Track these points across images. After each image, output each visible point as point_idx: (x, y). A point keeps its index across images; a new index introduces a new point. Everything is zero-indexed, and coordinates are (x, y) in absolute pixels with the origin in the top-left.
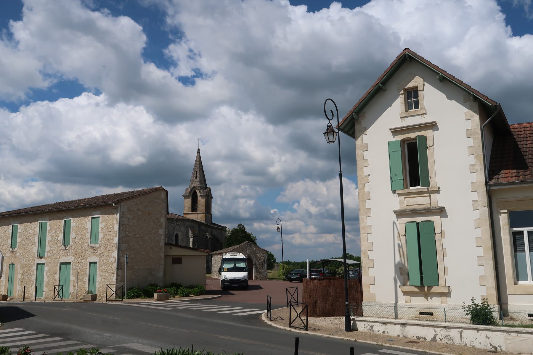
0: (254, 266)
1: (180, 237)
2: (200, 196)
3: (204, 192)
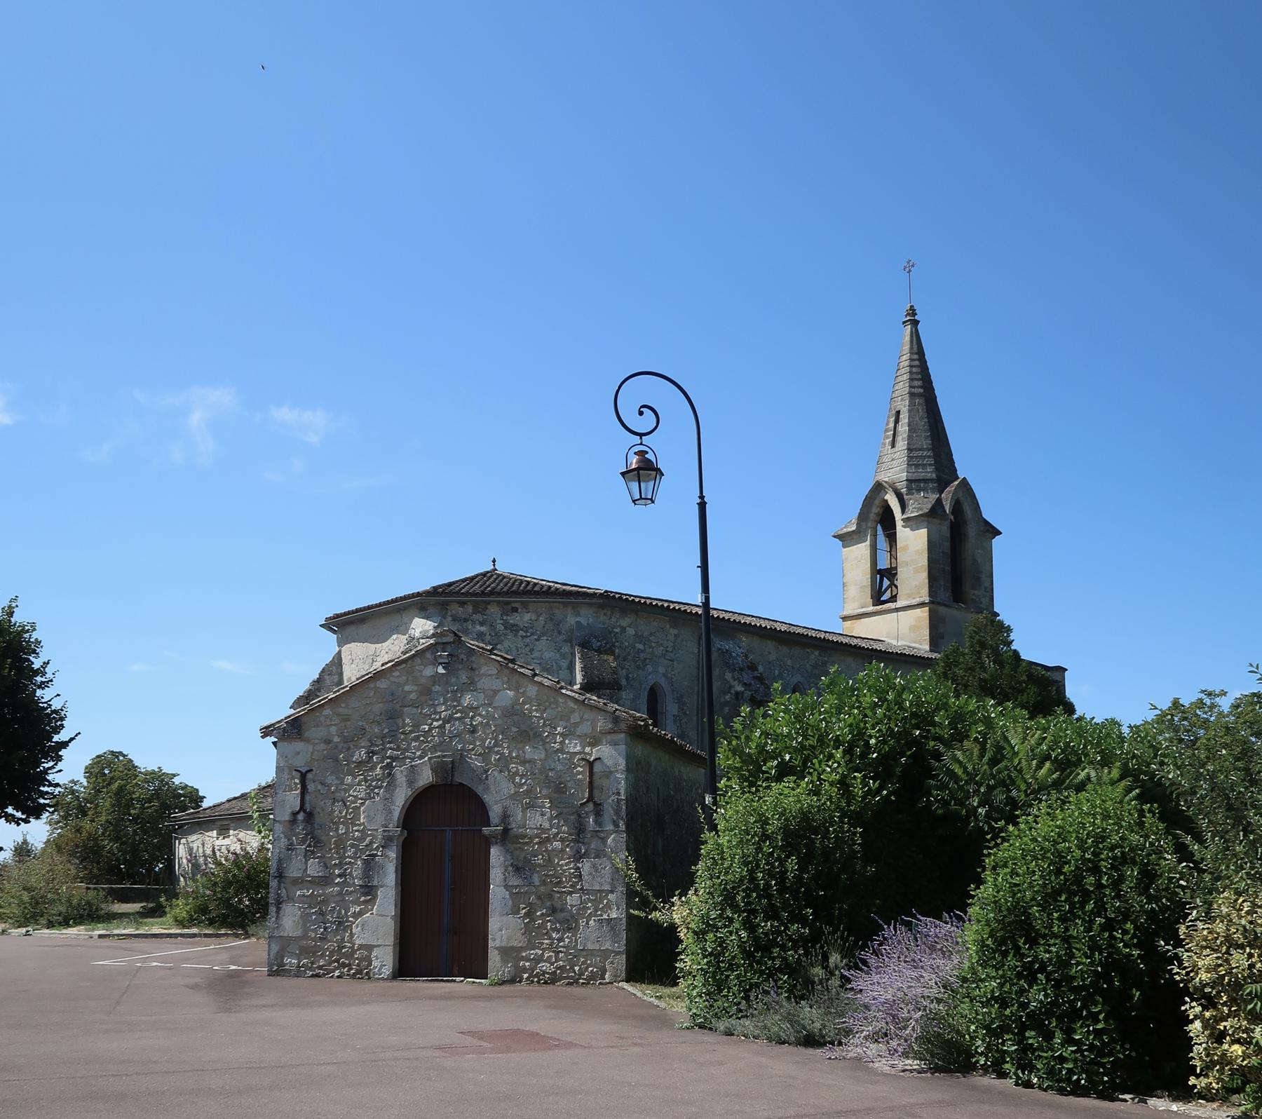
0: (496, 854)
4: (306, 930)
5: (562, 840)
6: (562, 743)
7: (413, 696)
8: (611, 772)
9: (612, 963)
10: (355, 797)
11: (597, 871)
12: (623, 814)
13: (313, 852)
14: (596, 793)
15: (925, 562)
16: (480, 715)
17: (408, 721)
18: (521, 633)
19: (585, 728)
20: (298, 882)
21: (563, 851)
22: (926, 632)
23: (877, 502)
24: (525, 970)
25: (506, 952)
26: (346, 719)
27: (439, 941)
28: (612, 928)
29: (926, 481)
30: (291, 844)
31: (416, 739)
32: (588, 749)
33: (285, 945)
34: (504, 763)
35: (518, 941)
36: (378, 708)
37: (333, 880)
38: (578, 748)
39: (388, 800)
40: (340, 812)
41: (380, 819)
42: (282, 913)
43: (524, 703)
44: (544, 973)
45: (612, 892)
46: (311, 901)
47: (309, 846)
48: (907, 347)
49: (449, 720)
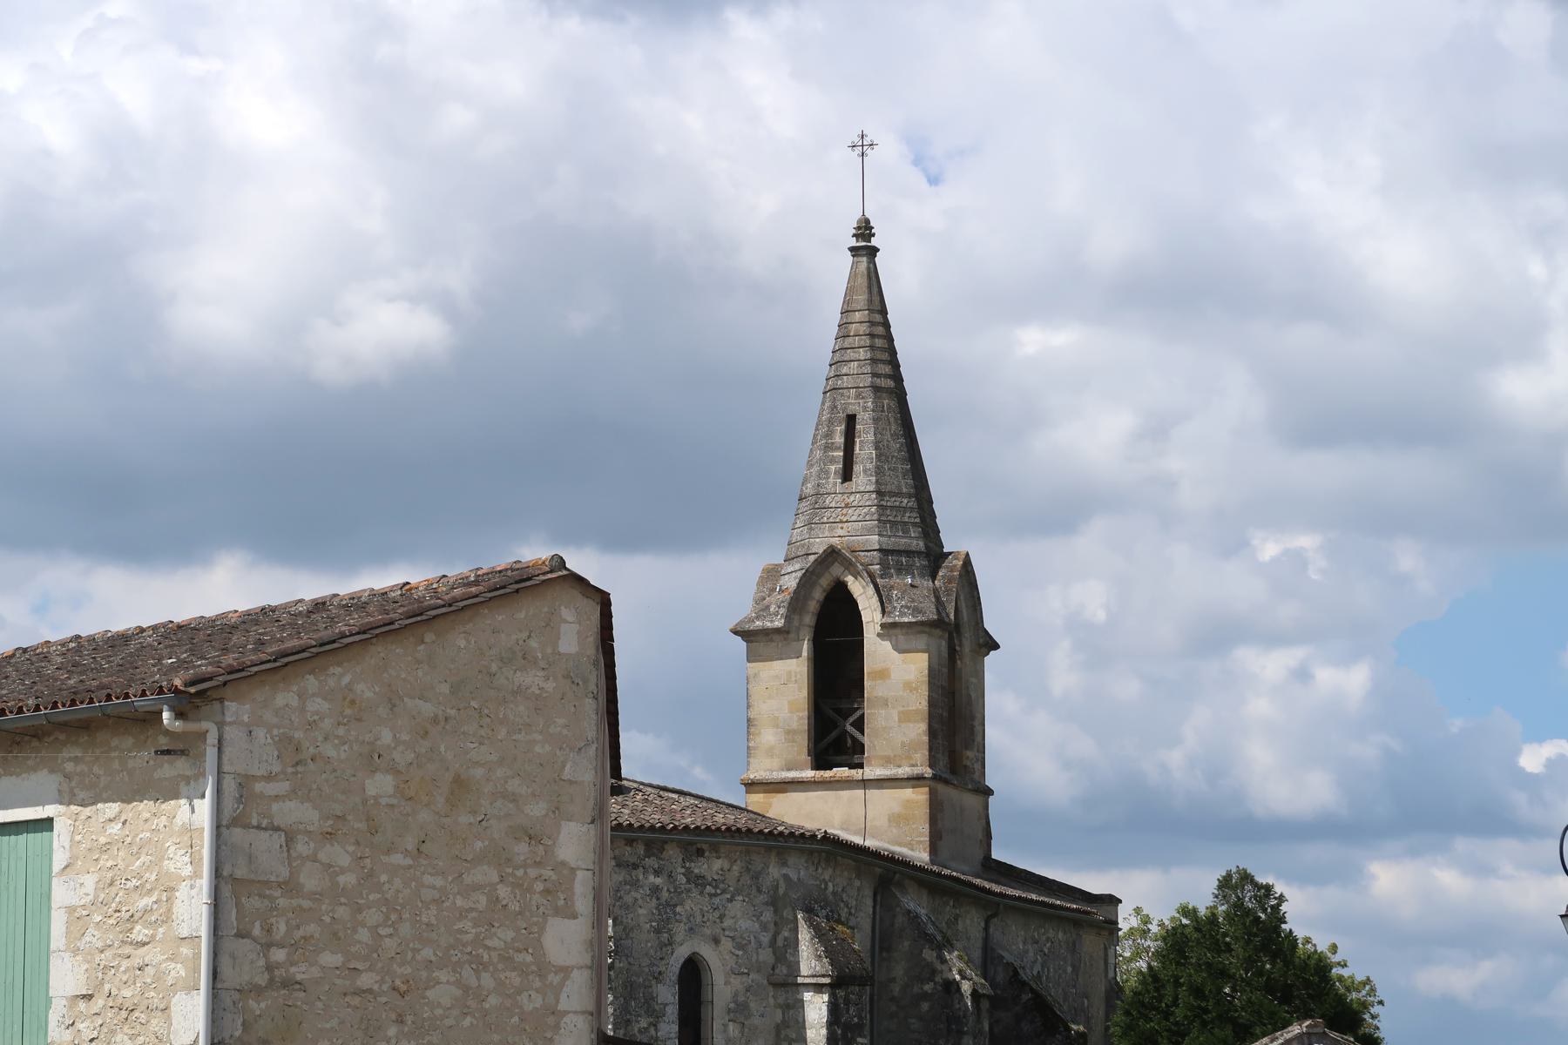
1: (722, 988)
2: (888, 629)
3: (916, 595)
22: (923, 828)
23: (825, 582)
29: (909, 553)
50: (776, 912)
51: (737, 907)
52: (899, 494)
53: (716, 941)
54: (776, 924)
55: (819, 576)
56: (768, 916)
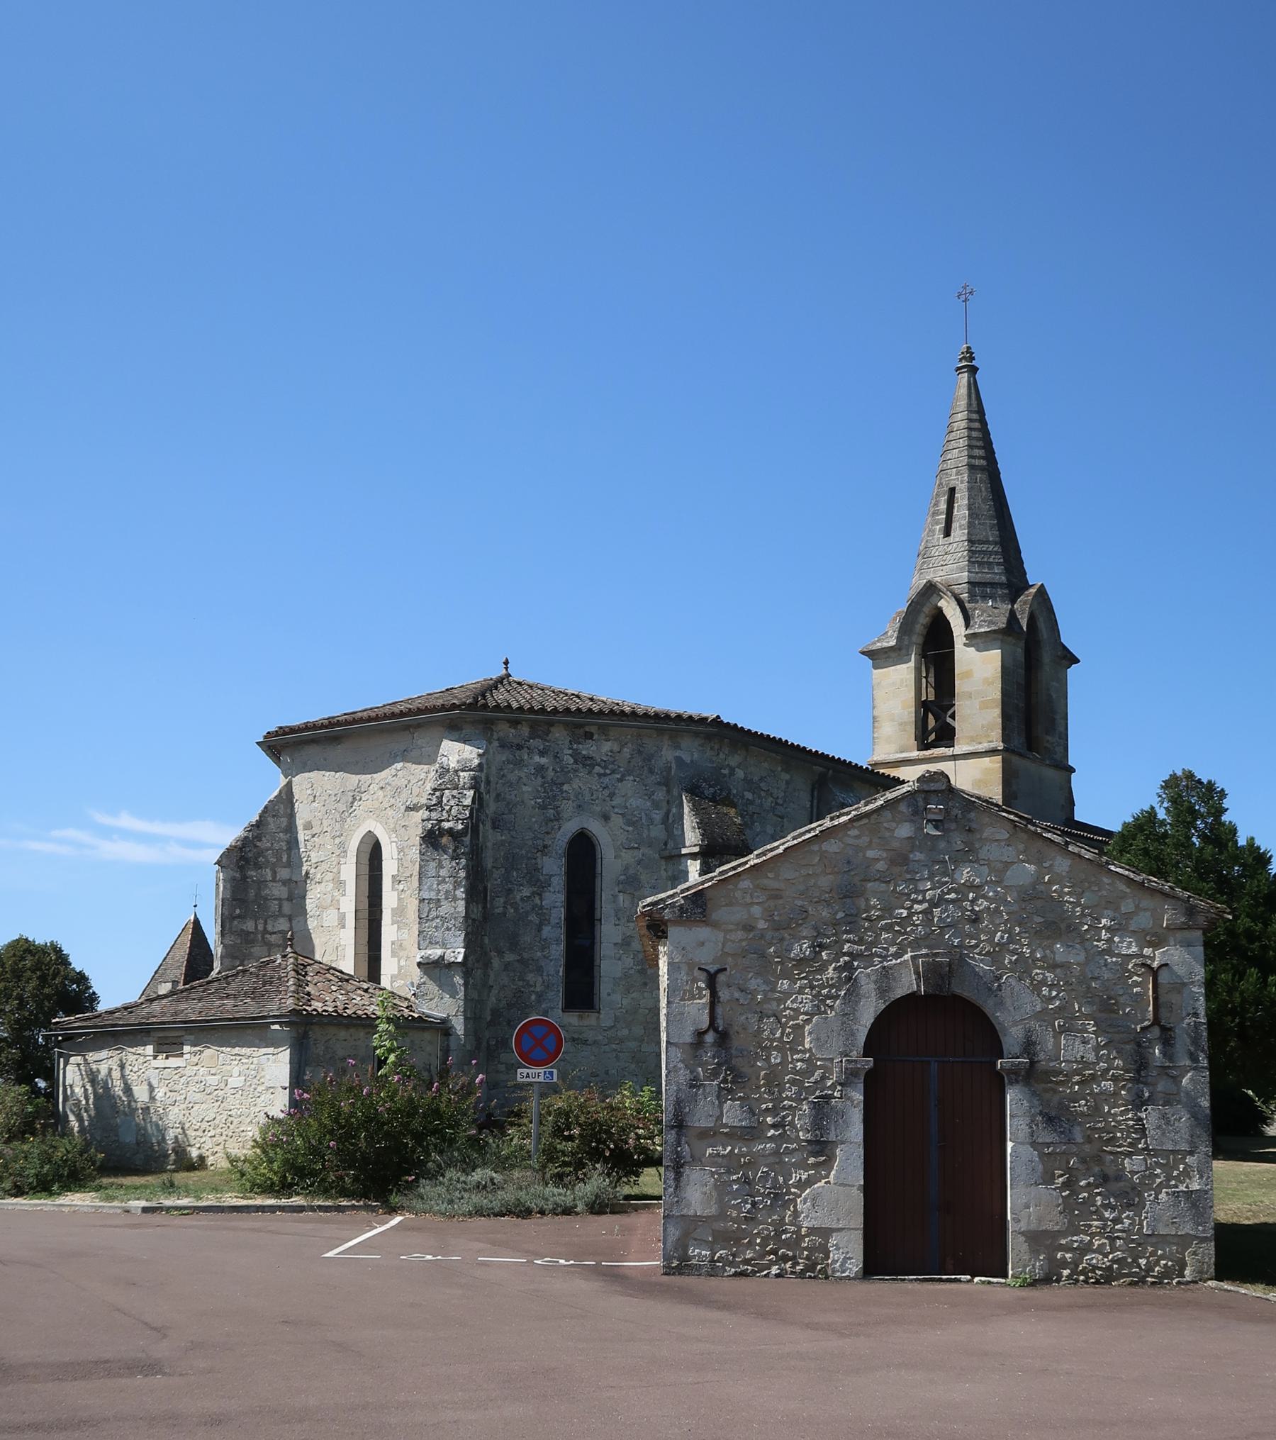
0: (1013, 1098)
1: (612, 861)
2: (972, 639)
3: (991, 615)
4: (723, 1207)
5: (1115, 1079)
6: (1110, 941)
7: (881, 866)
8: (1184, 984)
9: (1195, 1253)
10: (796, 1010)
11: (1168, 1123)
12: (1204, 1042)
13: (730, 1091)
14: (1164, 1013)
15: (998, 695)
16: (985, 897)
17: (874, 901)
18: (597, 769)
19: (1143, 921)
20: (707, 1135)
21: (1116, 1094)
23: (926, 609)
24: (1064, 1264)
25: (1036, 1239)
26: (776, 895)
27: (931, 1219)
28: (1194, 1205)
29: (992, 585)
30: (696, 1078)
31: (888, 928)
32: (1147, 951)
33: (689, 1227)
34: (1023, 967)
35: (1054, 1222)
36: (825, 881)
37: (764, 1132)
38: (1134, 949)
39: (848, 1016)
40: (773, 1032)
41: (837, 1044)
42: (684, 1179)
43: (1051, 882)
44: (1095, 1268)
45: (1191, 1153)
46: (731, 1163)
47: (725, 1081)
48: (963, 403)
49: (934, 904)
50: (668, 791)
51: (628, 785)
52: (987, 542)
53: (606, 818)
54: (668, 802)
55: (923, 606)
56: (660, 794)
